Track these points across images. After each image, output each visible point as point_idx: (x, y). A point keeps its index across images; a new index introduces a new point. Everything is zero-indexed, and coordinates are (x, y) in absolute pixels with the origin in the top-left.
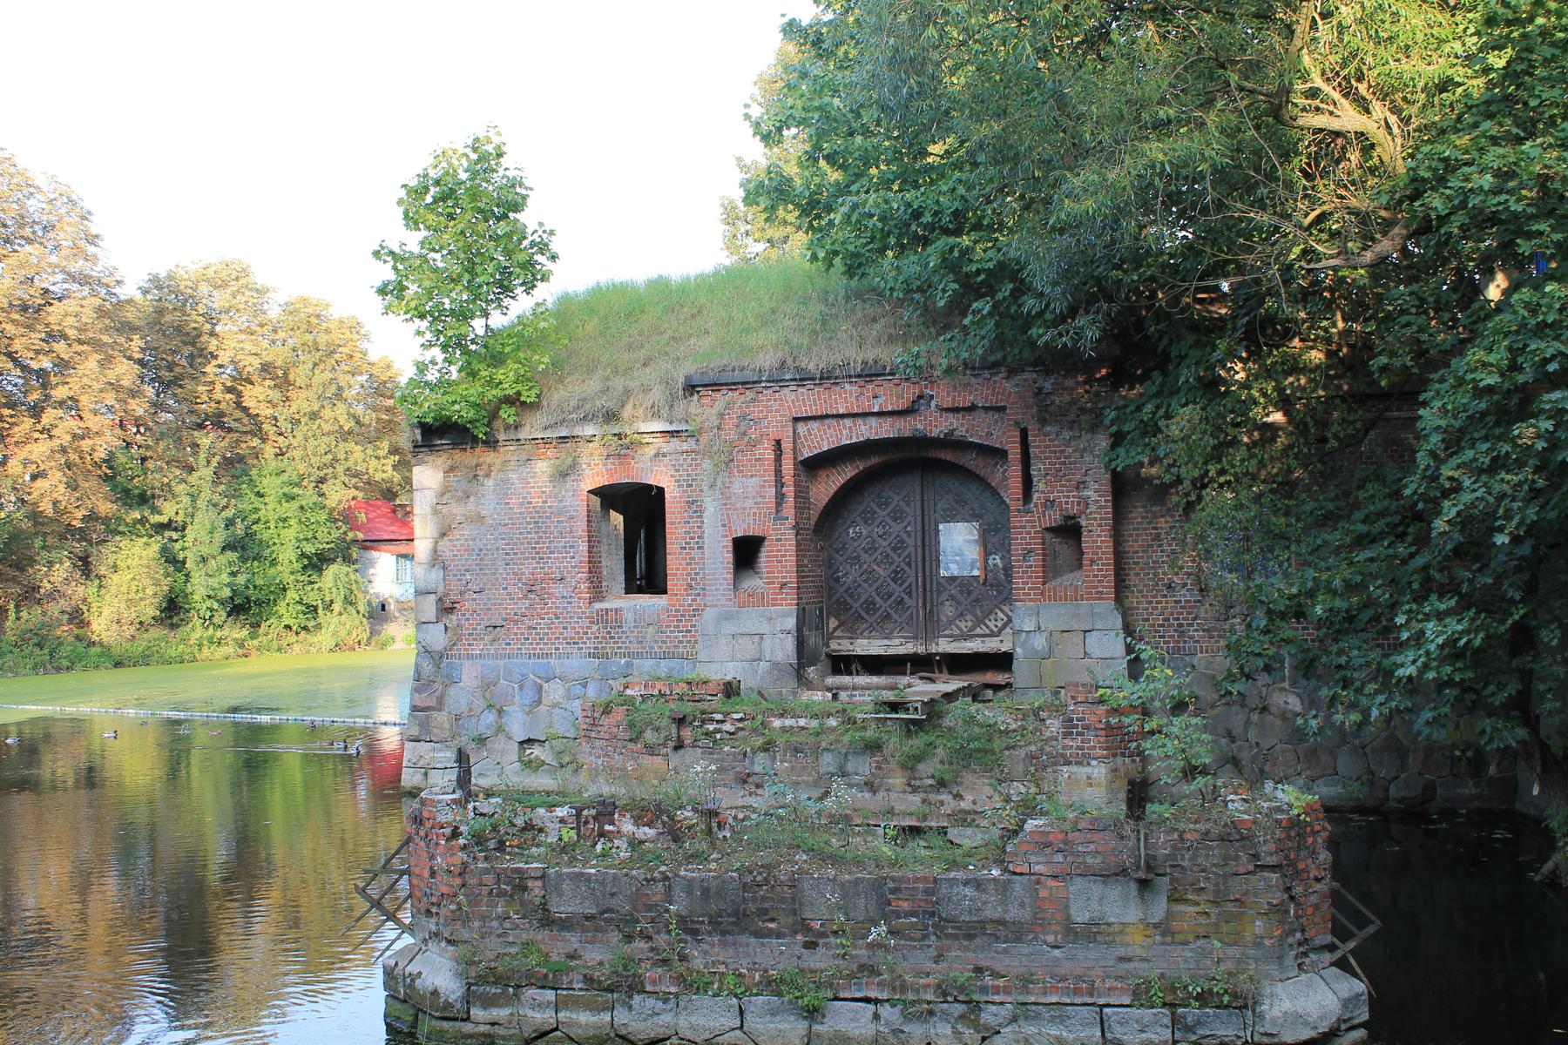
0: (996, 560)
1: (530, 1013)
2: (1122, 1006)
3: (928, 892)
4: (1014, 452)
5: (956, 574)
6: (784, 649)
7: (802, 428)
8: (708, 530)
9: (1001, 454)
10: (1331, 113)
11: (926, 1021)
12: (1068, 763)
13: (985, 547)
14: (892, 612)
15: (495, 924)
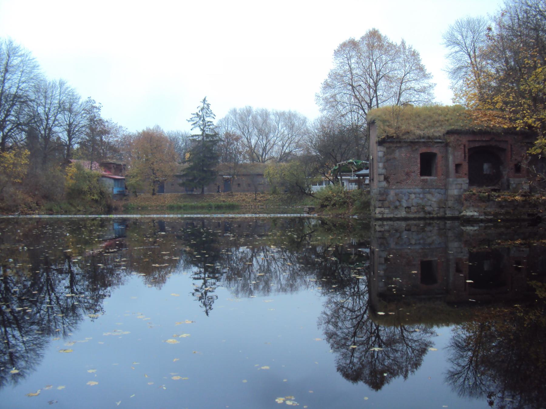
10: (213, 118)
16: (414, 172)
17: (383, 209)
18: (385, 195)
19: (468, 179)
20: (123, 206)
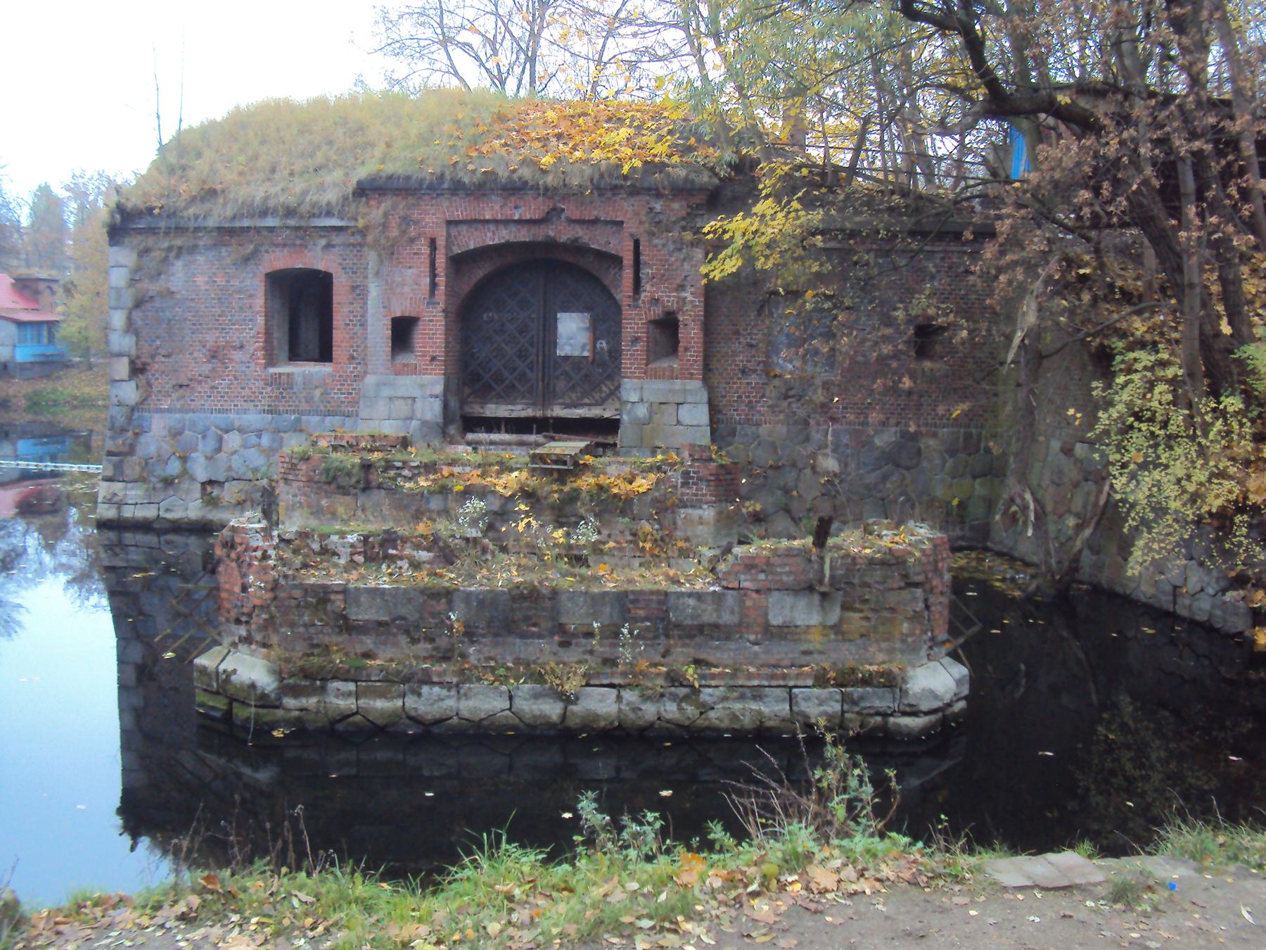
0: (603, 344)
1: (335, 701)
2: (806, 687)
3: (659, 602)
4: (628, 259)
5: (569, 354)
6: (431, 410)
7: (454, 231)
8: (371, 311)
9: (616, 260)
11: (658, 701)
12: (685, 506)
13: (594, 334)
14: (516, 383)
15: (301, 630)
16: (242, 347)
17: (120, 485)
18: (130, 434)
19: (441, 379)
20: (28, 397)
